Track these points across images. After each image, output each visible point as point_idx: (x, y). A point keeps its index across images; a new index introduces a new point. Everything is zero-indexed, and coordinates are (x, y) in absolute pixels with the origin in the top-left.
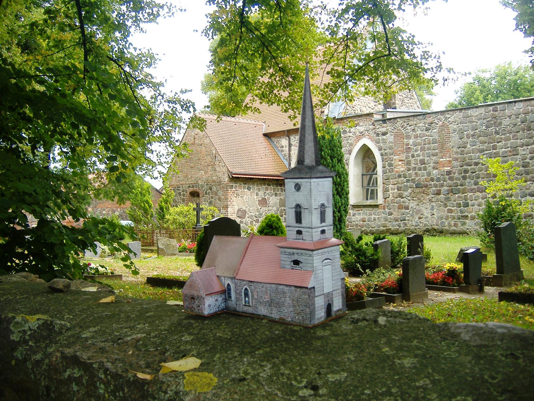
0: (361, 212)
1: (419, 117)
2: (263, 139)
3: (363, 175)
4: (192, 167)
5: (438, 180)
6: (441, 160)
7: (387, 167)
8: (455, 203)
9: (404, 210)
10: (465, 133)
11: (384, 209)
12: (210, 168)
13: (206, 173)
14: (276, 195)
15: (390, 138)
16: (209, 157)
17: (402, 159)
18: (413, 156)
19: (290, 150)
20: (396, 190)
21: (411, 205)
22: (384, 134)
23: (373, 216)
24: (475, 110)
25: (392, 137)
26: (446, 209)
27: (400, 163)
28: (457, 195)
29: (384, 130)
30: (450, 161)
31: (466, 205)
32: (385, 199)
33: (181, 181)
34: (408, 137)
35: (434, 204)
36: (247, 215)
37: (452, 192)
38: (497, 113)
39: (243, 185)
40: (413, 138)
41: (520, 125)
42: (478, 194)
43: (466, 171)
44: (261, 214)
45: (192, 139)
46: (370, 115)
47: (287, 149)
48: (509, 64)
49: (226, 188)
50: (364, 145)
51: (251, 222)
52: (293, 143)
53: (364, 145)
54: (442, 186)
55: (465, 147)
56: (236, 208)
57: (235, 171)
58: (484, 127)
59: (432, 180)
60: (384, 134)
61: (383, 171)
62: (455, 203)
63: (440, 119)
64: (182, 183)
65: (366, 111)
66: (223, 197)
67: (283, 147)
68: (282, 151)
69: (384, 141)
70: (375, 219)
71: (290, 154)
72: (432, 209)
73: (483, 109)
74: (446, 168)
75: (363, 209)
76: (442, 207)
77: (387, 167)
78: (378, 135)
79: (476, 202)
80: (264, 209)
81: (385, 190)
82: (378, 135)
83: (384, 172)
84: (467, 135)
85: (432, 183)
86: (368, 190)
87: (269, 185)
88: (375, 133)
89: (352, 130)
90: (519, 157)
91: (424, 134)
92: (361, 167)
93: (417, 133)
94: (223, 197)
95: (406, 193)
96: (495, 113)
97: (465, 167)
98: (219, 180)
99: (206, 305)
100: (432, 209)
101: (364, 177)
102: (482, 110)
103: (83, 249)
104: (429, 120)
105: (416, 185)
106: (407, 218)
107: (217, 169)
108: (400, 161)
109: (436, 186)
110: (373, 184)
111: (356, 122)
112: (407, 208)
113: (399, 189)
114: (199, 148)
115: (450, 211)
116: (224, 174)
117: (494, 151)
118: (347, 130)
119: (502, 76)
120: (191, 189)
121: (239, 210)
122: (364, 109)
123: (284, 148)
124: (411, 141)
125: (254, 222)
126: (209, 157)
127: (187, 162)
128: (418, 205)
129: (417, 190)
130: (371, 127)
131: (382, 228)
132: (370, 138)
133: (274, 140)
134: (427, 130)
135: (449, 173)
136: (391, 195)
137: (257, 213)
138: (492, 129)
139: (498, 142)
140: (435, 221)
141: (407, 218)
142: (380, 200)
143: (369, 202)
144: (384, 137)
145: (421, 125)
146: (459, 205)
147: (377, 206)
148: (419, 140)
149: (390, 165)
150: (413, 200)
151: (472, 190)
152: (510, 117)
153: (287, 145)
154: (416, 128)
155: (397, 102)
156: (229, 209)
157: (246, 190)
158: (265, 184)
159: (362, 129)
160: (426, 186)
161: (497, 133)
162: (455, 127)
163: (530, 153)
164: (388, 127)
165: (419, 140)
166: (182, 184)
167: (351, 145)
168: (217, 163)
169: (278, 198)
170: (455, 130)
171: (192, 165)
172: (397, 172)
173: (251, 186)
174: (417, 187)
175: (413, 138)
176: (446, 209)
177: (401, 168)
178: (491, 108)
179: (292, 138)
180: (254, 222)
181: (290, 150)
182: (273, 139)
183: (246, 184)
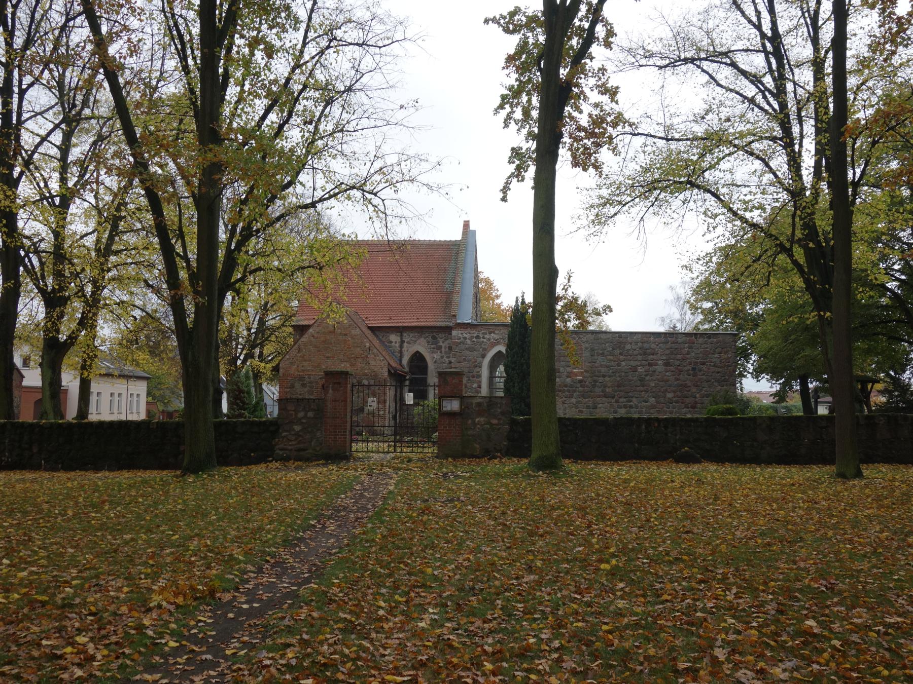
4: (328, 358)
5: (571, 386)
31: (595, 407)
43: (595, 381)
48: (608, 309)
50: (418, 352)
54: (575, 391)
59: (566, 386)
67: (391, 342)
71: (401, 352)
89: (487, 336)
103: (830, 409)
118: (481, 336)
138: (617, 352)
146: (588, 407)
159: (496, 337)
167: (484, 349)
170: (587, 348)
179: (405, 334)
182: (378, 333)
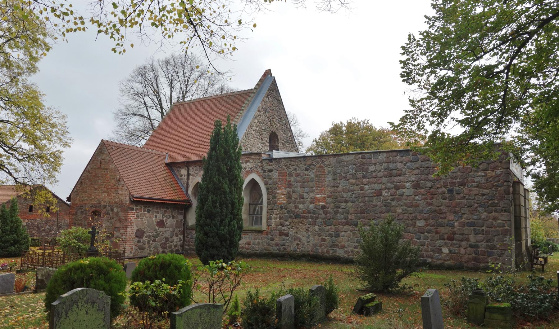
0: (247, 236)
1: (300, 159)
2: (163, 167)
3: (250, 204)
4: (96, 189)
5: (314, 213)
6: (317, 196)
7: (271, 199)
8: (328, 233)
9: (284, 237)
10: (338, 175)
11: (267, 235)
12: (113, 190)
13: (109, 195)
14: (173, 217)
15: (275, 175)
16: (113, 181)
17: (284, 193)
18: (294, 192)
19: (188, 179)
20: (278, 219)
21: (290, 233)
22: (270, 171)
23: (257, 241)
24: (346, 156)
25: (277, 174)
26: (320, 238)
27: (283, 196)
28: (329, 227)
29: (270, 167)
30: (324, 197)
32: (269, 226)
33: (84, 200)
34: (290, 175)
35: (310, 233)
36: (145, 235)
37: (325, 223)
38: (365, 160)
39: (143, 208)
40: (294, 176)
41: (383, 172)
42: (347, 227)
44: (159, 234)
45: (99, 163)
46: (259, 154)
47: (186, 177)
49: (127, 210)
50: (253, 179)
51: (149, 242)
52: (191, 173)
53: (253, 179)
55: (337, 187)
56: (135, 228)
57: (135, 194)
58: (354, 171)
59: (309, 212)
60: (270, 171)
61: (268, 202)
62: (328, 233)
63: (318, 162)
64: (85, 202)
65: (255, 150)
66: (123, 218)
67: (182, 175)
68: (182, 179)
69: (270, 177)
70: (259, 243)
72: (308, 237)
73: (354, 156)
74: (321, 203)
75: (250, 234)
76: (317, 236)
77: (271, 199)
78: (265, 171)
79: (346, 234)
80: (161, 229)
81: (269, 219)
82: (265, 171)
83: (269, 203)
84: (340, 177)
85: (309, 215)
86: (253, 217)
87: (167, 208)
88: (262, 169)
90: (382, 197)
91: (304, 173)
92: (249, 197)
93: (298, 172)
94: (123, 218)
95: (287, 223)
96: (363, 160)
97: (337, 203)
98: (120, 202)
99: (132, 230)
100: (308, 237)
101: (251, 206)
102: (352, 157)
104: (309, 162)
105: (295, 216)
106: (287, 244)
107: (120, 192)
108: (283, 194)
109: (312, 218)
110: (257, 212)
111: (247, 159)
112: (287, 235)
113: (280, 218)
114: (104, 172)
115: (324, 240)
116: (126, 197)
117: (362, 192)
119: (350, 125)
120: (93, 209)
121: (138, 230)
122: (253, 149)
123: (183, 177)
124: (292, 179)
125: (151, 242)
126: (113, 181)
127: (91, 184)
128: (297, 233)
129: (296, 220)
130: (259, 164)
131: (265, 251)
132: (258, 173)
133: (175, 169)
134: (307, 170)
135: (323, 207)
136: (274, 223)
137: (155, 233)
138: (360, 174)
139: (365, 185)
140: (310, 248)
141: (287, 244)
142: (264, 227)
143: (255, 227)
144: (270, 174)
145: (301, 165)
146: (330, 235)
147: (260, 232)
148: (299, 179)
149: (274, 197)
150: (292, 228)
151: (342, 224)
152: (375, 164)
153: (186, 174)
154: (297, 168)
155: (279, 145)
156: (128, 230)
157: (146, 212)
158: (163, 208)
160: (304, 217)
161: (364, 177)
162: (330, 169)
163: (391, 195)
164: (273, 165)
165: (299, 179)
166: (85, 204)
168: (120, 187)
169: (175, 220)
170: (329, 172)
171: (96, 187)
172: (279, 204)
173: (151, 209)
174: (296, 218)
175: (294, 176)
176: (320, 238)
177: (282, 200)
178: (360, 156)
179: (191, 168)
180: (151, 242)
181: (188, 179)
183: (146, 207)
